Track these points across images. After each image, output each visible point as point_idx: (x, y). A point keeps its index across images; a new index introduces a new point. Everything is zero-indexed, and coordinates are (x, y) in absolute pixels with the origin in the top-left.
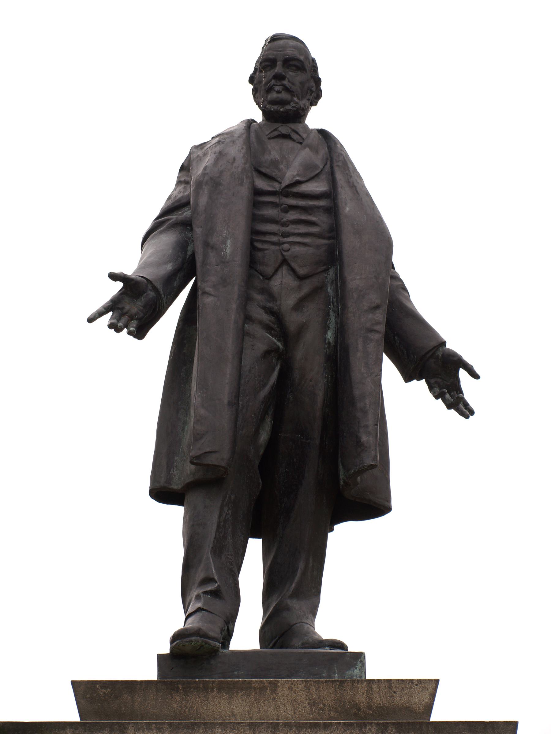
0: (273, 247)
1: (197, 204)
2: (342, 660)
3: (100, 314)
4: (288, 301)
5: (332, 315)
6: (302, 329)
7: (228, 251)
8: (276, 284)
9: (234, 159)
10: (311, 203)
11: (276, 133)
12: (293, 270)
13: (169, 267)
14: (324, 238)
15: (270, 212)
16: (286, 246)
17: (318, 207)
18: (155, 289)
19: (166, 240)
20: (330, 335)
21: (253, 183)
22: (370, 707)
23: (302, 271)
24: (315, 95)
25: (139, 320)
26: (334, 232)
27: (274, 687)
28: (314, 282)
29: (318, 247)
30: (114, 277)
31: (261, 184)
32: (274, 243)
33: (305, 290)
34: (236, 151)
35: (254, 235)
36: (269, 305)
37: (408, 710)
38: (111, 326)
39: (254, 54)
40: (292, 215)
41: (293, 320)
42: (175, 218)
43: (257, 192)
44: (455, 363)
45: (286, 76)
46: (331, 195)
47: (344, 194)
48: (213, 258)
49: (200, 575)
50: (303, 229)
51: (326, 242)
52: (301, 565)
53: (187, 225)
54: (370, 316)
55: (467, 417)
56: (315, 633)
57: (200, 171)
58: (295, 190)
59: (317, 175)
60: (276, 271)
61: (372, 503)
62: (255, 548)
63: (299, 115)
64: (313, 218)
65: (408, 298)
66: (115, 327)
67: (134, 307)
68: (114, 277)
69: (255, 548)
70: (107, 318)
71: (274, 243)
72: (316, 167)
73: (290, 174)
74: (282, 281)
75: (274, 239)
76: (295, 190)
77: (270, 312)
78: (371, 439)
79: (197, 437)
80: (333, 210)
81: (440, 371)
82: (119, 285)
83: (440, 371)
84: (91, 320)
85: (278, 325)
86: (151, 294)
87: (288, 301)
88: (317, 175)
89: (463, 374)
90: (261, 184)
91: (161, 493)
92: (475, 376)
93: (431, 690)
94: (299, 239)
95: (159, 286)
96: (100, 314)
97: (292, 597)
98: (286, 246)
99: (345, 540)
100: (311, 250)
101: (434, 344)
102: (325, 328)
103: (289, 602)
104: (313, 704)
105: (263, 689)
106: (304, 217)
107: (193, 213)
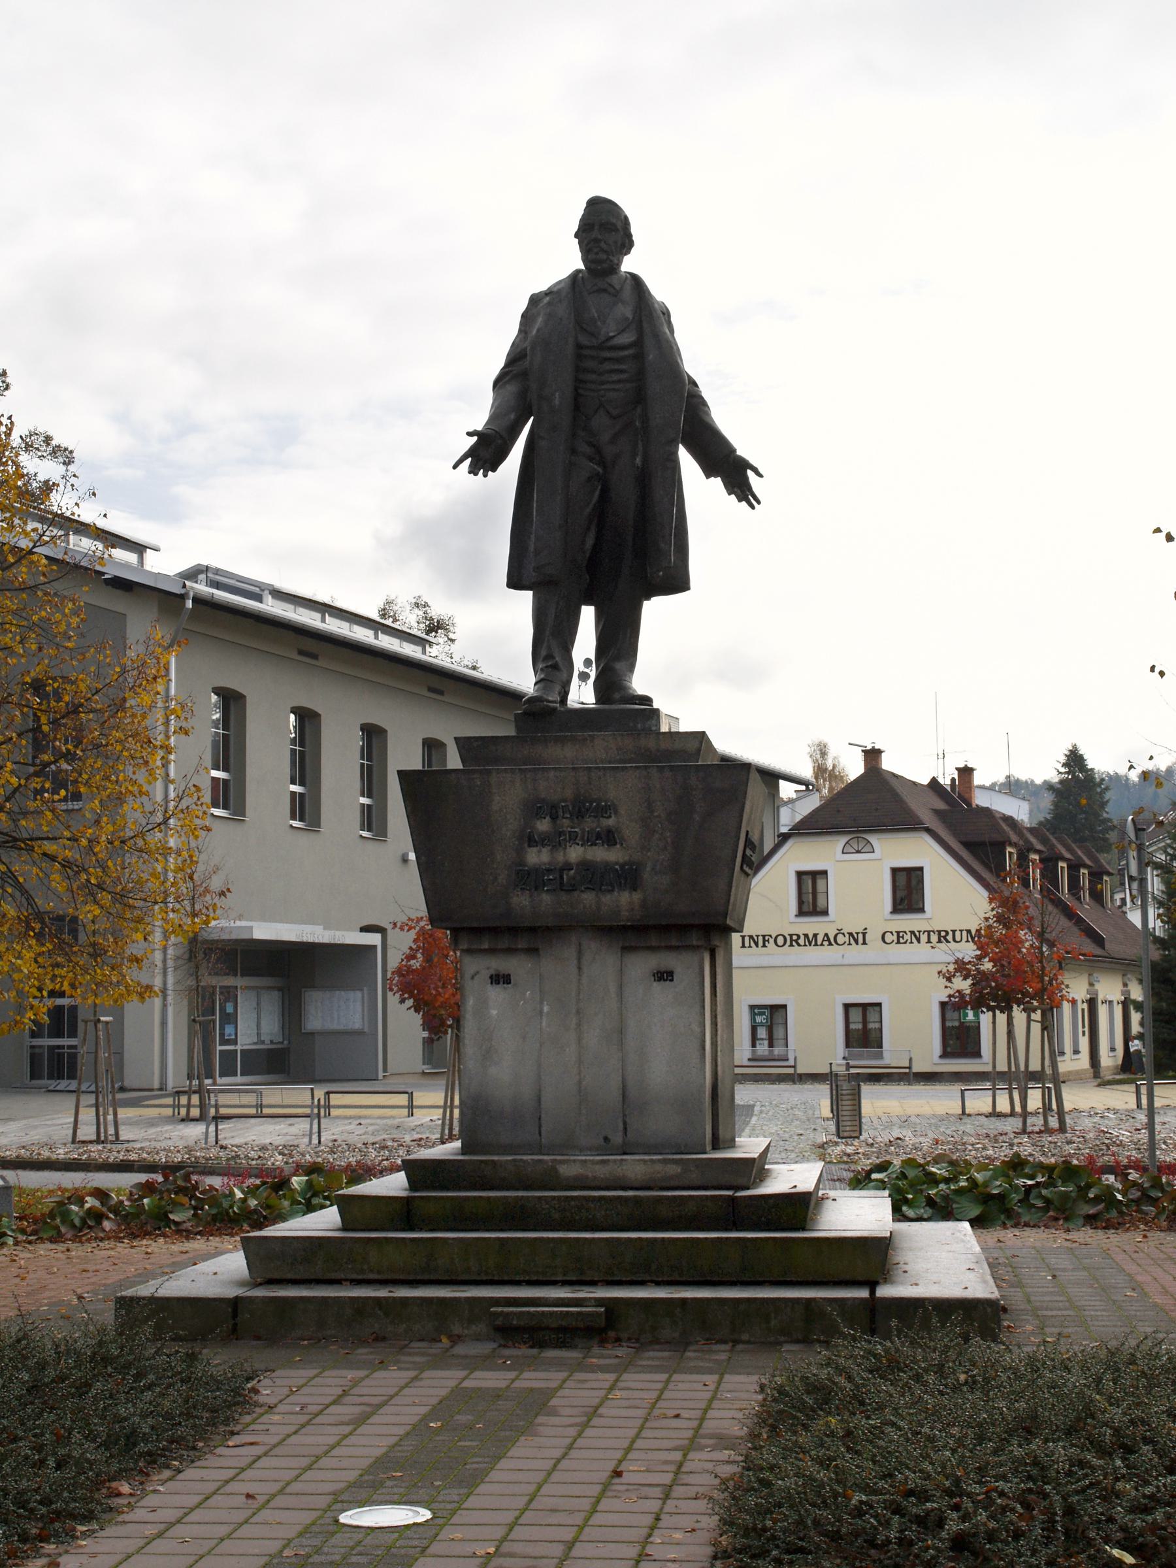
2: (644, 712)
4: (605, 437)
7: (557, 402)
15: (590, 364)
18: (501, 437)
19: (511, 388)
20: (638, 461)
21: (576, 338)
22: (658, 750)
23: (615, 412)
26: (640, 376)
30: (470, 434)
31: (584, 340)
34: (562, 310)
35: (578, 383)
39: (578, 211)
40: (608, 366)
43: (579, 346)
44: (741, 466)
45: (604, 229)
46: (639, 343)
47: (649, 342)
49: (544, 653)
50: (615, 377)
53: (524, 375)
55: (753, 507)
56: (630, 688)
57: (534, 332)
60: (596, 411)
61: (675, 581)
62: (588, 613)
63: (614, 268)
65: (708, 414)
66: (473, 471)
68: (470, 434)
69: (588, 613)
72: (627, 319)
74: (600, 421)
75: (593, 386)
77: (590, 444)
79: (537, 553)
80: (639, 357)
81: (734, 473)
82: (475, 438)
83: (734, 473)
84: (455, 467)
85: (598, 456)
87: (605, 437)
89: (750, 473)
91: (515, 581)
92: (760, 475)
94: (613, 386)
99: (656, 612)
100: (629, 385)
102: (634, 456)
105: (585, 740)
106: (616, 367)
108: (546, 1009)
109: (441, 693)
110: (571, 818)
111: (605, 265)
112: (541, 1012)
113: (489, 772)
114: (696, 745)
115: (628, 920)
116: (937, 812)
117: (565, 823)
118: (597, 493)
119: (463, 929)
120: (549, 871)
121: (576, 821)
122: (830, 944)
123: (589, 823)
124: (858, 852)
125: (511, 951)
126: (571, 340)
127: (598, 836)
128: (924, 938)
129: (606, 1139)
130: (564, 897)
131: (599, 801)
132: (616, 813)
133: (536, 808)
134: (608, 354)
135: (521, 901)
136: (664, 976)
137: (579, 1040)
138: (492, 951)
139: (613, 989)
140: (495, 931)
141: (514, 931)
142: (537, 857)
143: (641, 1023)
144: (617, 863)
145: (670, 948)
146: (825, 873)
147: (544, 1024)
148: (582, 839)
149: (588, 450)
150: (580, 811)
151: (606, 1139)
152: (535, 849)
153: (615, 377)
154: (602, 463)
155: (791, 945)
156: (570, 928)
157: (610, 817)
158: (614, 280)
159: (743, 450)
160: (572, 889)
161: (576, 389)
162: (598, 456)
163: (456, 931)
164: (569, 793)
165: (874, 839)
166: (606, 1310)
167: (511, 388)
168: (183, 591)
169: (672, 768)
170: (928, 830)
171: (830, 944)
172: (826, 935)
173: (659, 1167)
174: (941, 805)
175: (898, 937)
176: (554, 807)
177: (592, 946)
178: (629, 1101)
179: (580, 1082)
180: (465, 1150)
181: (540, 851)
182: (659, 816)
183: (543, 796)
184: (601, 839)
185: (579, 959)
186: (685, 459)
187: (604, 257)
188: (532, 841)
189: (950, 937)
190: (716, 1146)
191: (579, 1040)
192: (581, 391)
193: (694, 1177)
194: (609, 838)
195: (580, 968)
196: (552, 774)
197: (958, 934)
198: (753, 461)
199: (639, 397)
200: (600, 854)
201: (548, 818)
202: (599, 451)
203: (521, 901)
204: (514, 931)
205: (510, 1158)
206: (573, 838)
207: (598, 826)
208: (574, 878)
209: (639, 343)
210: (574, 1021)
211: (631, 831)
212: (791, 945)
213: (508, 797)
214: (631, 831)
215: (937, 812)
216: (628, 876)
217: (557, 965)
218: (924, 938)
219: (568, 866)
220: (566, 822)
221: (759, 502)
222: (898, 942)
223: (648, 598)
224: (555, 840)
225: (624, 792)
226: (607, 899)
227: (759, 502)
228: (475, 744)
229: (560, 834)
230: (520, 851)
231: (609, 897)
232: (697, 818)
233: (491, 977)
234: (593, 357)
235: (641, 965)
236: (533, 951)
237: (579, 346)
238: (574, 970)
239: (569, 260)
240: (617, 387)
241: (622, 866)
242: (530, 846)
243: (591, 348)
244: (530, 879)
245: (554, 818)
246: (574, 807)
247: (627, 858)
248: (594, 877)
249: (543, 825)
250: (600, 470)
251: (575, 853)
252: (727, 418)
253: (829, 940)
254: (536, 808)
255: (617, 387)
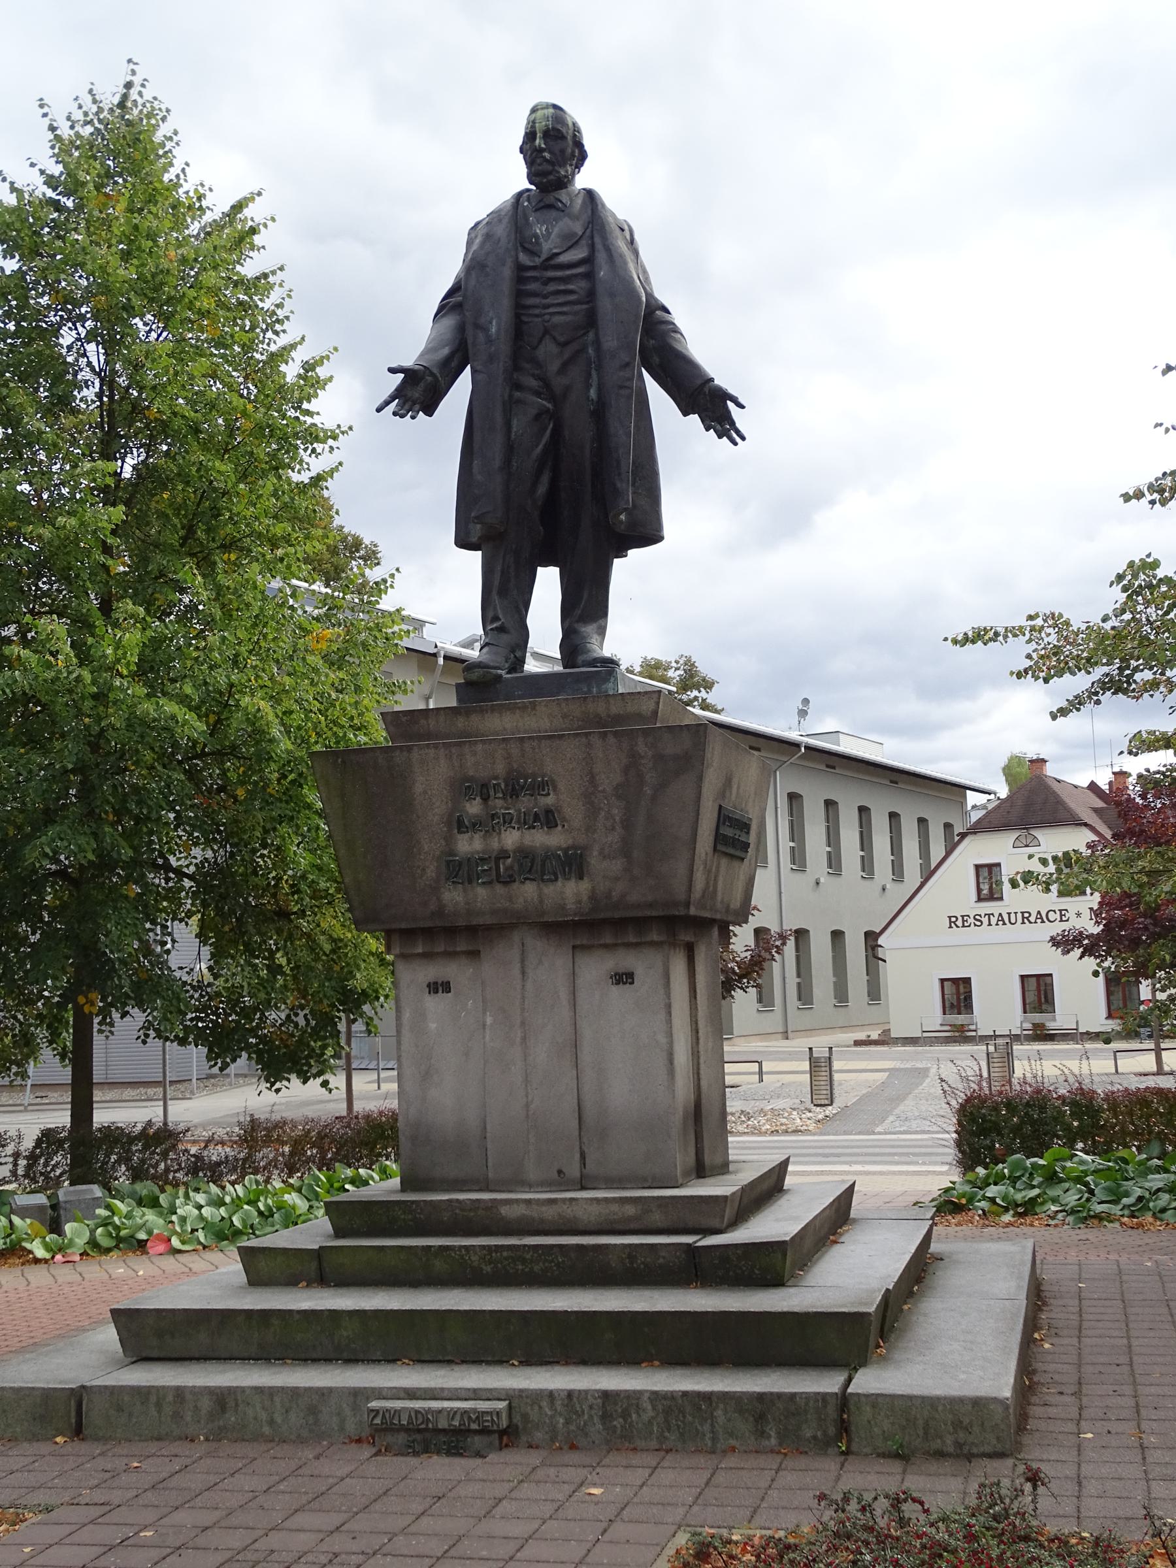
0: (536, 320)
1: (466, 290)
3: (387, 403)
5: (594, 373)
6: (567, 389)
8: (541, 353)
9: (499, 240)
10: (568, 272)
11: (542, 204)
12: (554, 338)
13: (446, 351)
14: (582, 303)
15: (532, 286)
16: (547, 317)
17: (576, 276)
18: (432, 374)
19: (449, 322)
20: (593, 393)
22: (609, 716)
24: (580, 156)
25: (422, 403)
27: (534, 706)
28: (575, 346)
29: (575, 313)
30: (392, 371)
31: (523, 258)
32: (537, 316)
33: (566, 356)
35: (519, 311)
36: (536, 372)
37: (639, 717)
38: (395, 414)
40: (552, 287)
41: (559, 383)
42: (454, 303)
43: (520, 268)
45: (553, 147)
46: (589, 260)
47: (601, 257)
48: (481, 337)
49: (491, 614)
50: (561, 299)
51: (585, 306)
52: (585, 596)
54: (622, 374)
55: (735, 444)
58: (552, 262)
59: (576, 243)
60: (540, 341)
61: (647, 532)
63: (564, 183)
64: (571, 287)
67: (416, 393)
68: (392, 371)
70: (393, 406)
71: (537, 316)
73: (547, 247)
74: (548, 350)
75: (537, 311)
76: (552, 262)
78: (624, 485)
80: (590, 276)
81: (711, 405)
82: (400, 377)
83: (711, 405)
84: (379, 410)
85: (546, 389)
86: (429, 379)
87: (554, 366)
88: (576, 243)
90: (523, 258)
93: (655, 699)
95: (435, 371)
96: (387, 403)
97: (578, 622)
98: (547, 317)
100: (577, 308)
101: (699, 382)
102: (588, 386)
103: (576, 625)
104: (564, 716)
106: (562, 287)
107: (464, 296)
108: (489, 1020)
109: (834, 768)
110: (504, 798)
111: (551, 177)
112: (484, 1025)
113: (409, 749)
114: (652, 706)
115: (575, 915)
116: (1096, 810)
117: (498, 804)
118: (548, 432)
119: (395, 930)
120: (483, 860)
121: (510, 801)
122: (1043, 922)
123: (525, 803)
124: (1027, 846)
125: (452, 955)
126: (509, 263)
127: (536, 817)
128: (985, 920)
129: (560, 1172)
130: (500, 889)
131: (534, 776)
132: (555, 788)
133: (466, 787)
134: (551, 274)
135: (453, 897)
136: (624, 978)
137: (525, 1056)
138: (428, 956)
139: (564, 994)
140: (428, 933)
141: (451, 932)
142: (468, 845)
143: (616, 1028)
144: (560, 848)
145: (628, 945)
146: (999, 865)
147: (487, 1037)
148: (518, 822)
149: (534, 383)
150: (513, 789)
151: (560, 1172)
152: (466, 836)
153: (561, 299)
154: (552, 398)
155: (1023, 923)
156: (512, 927)
157: (548, 794)
158: (563, 195)
159: (722, 380)
160: (508, 881)
161: (517, 316)
162: (546, 389)
163: (389, 934)
164: (500, 768)
165: (1038, 834)
166: (510, 1407)
167: (449, 322)
168: (435, 651)
169: (615, 734)
170: (1086, 825)
171: (1043, 922)
172: (1039, 912)
173: (615, 1207)
174: (1100, 804)
175: (1061, 915)
176: (484, 786)
177: (536, 945)
178: (587, 1124)
179: (527, 1105)
180: (406, 1186)
181: (471, 838)
182: (604, 791)
183: (471, 773)
184: (540, 821)
185: (523, 961)
186: (655, 391)
187: (550, 168)
188: (461, 826)
189: (959, 923)
190: (701, 1171)
191: (525, 1056)
192: (525, 319)
193: (657, 1218)
194: (549, 819)
195: (523, 973)
196: (480, 747)
197: (1013, 916)
198: (732, 391)
199: (591, 320)
200: (540, 839)
201: (478, 799)
202: (547, 384)
203: (453, 897)
204: (451, 932)
205: (445, 1197)
206: (507, 821)
207: (536, 805)
208: (511, 867)
209: (589, 260)
210: (519, 1034)
211: (573, 810)
212: (1023, 923)
213: (431, 778)
214: (573, 810)
215: (1096, 810)
216: (572, 863)
217: (498, 969)
218: (985, 920)
219: (503, 854)
220: (499, 803)
221: (743, 438)
222: (1061, 921)
223: (621, 553)
224: (489, 824)
225: (563, 767)
226: (550, 890)
227: (743, 438)
228: (404, 719)
229: (493, 817)
230: (449, 839)
231: (552, 887)
232: (648, 791)
233: (429, 986)
234: (535, 279)
235: (594, 968)
236: (474, 954)
237: (520, 268)
238: (516, 971)
239: (513, 177)
240: (565, 309)
241: (566, 850)
242: (460, 832)
243: (534, 268)
244: (460, 871)
245: (485, 799)
246: (506, 785)
247: (570, 842)
248: (531, 865)
249: (474, 808)
250: (549, 406)
251: (511, 838)
252: (705, 344)
253: (1003, 920)
254: (466, 787)
255: (565, 309)
